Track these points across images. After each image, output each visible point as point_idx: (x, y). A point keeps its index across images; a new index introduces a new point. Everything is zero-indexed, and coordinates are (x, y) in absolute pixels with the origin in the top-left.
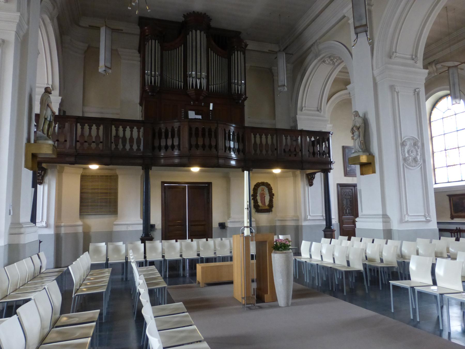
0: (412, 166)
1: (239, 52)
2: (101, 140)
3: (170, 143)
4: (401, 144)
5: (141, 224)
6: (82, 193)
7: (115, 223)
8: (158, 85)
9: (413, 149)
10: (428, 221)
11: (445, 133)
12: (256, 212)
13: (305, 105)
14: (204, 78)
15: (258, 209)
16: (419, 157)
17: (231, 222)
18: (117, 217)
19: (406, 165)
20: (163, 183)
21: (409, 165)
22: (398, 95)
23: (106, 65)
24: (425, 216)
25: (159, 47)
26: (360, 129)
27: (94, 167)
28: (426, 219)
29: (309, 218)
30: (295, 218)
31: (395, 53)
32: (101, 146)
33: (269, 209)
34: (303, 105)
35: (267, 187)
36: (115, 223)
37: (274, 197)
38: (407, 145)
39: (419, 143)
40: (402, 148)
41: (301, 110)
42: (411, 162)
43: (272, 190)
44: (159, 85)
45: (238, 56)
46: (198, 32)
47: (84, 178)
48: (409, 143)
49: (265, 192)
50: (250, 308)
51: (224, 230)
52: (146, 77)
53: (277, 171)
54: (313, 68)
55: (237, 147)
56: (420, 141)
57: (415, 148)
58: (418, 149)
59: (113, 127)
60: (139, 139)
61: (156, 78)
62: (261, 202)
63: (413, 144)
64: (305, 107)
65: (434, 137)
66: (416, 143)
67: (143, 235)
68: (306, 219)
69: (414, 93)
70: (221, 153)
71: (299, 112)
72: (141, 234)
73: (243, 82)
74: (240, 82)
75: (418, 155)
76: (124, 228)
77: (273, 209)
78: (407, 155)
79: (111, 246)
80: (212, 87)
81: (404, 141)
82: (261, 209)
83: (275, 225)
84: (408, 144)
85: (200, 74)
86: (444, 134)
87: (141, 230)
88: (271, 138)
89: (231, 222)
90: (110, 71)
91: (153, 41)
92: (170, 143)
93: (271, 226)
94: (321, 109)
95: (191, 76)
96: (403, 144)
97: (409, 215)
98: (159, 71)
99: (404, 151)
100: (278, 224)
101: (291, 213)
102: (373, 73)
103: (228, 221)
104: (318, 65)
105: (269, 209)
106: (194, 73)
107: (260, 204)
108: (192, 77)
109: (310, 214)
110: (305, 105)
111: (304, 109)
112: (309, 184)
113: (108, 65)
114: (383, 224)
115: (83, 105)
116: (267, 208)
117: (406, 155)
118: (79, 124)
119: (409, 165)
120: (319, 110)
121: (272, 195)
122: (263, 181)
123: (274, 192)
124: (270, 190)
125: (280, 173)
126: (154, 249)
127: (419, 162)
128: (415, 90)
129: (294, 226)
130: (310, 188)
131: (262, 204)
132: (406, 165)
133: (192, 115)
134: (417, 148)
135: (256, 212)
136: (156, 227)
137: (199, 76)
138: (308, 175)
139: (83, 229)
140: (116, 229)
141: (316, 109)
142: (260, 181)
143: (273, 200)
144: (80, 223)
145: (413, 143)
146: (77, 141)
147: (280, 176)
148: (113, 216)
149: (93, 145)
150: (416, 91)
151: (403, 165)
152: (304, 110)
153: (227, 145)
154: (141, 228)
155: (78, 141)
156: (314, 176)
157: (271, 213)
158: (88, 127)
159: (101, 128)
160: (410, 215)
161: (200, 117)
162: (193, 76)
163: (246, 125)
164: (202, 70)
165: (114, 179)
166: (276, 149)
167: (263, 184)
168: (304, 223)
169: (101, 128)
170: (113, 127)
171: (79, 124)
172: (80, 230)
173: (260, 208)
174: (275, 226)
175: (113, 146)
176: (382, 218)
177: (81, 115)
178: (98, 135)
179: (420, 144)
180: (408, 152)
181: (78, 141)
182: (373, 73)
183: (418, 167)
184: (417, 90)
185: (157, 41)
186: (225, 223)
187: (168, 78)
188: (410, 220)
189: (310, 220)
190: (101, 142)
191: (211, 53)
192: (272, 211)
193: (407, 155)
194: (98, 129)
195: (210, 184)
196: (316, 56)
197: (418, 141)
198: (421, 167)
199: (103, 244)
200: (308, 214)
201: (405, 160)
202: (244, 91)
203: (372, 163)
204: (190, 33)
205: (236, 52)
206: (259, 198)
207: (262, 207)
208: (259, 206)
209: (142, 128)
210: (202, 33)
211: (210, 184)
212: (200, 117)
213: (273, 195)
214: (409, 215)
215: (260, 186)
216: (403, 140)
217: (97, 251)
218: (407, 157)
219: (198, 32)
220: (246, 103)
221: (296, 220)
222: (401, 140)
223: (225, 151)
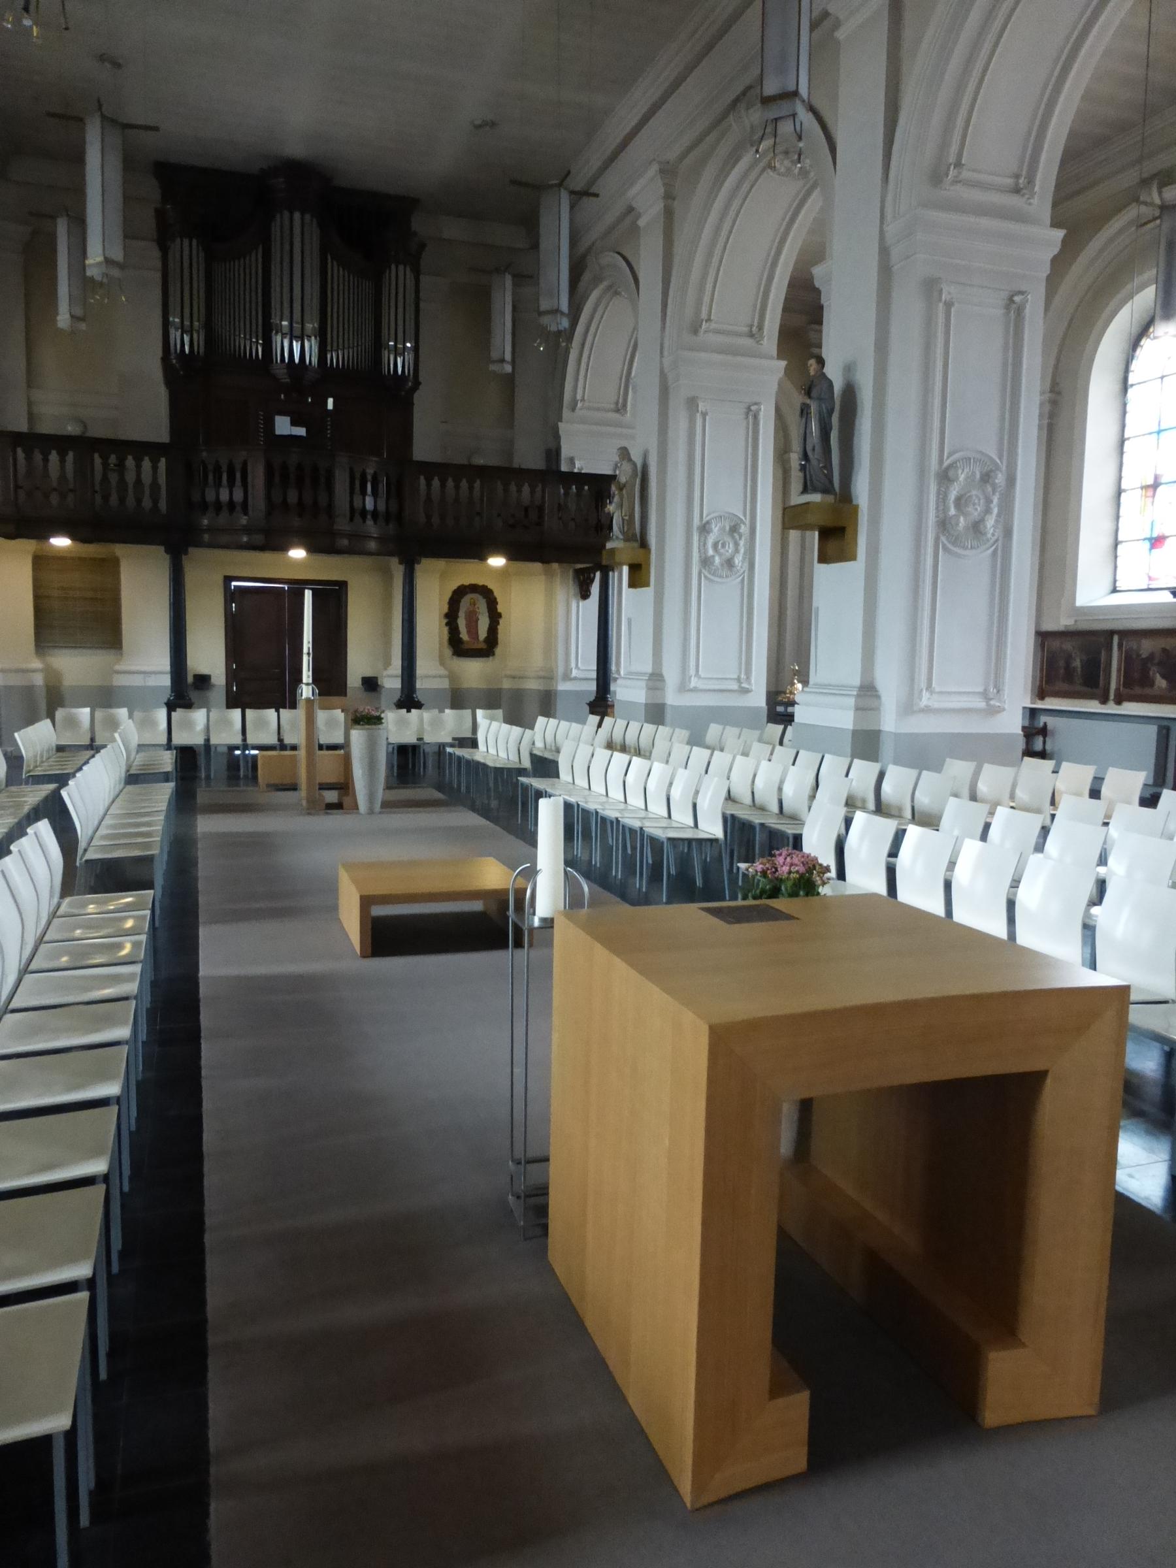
0: (721, 577)
1: (401, 267)
2: (71, 486)
3: (224, 496)
4: (698, 528)
5: (167, 673)
6: (37, 598)
7: (117, 667)
8: (198, 352)
9: (728, 539)
10: (746, 691)
11: (1162, 428)
12: (453, 655)
13: (583, 396)
14: (309, 334)
15: (458, 647)
16: (738, 560)
17: (389, 676)
18: (122, 654)
19: (946, 542)
20: (228, 579)
21: (956, 541)
22: (704, 420)
23: (73, 313)
24: (739, 680)
25: (202, 254)
26: (624, 492)
27: (61, 542)
28: (988, 704)
29: (575, 673)
30: (542, 674)
31: (706, 321)
32: (70, 498)
33: (489, 648)
34: (579, 397)
35: (484, 598)
36: (117, 667)
37: (501, 621)
38: (957, 479)
39: (1000, 475)
40: (942, 489)
41: (573, 409)
42: (719, 567)
43: (497, 603)
44: (202, 350)
45: (398, 276)
46: (297, 216)
47: (41, 562)
48: (968, 473)
49: (478, 608)
50: (309, 814)
51: (373, 694)
52: (172, 331)
53: (497, 562)
54: (595, 310)
55: (382, 507)
56: (748, 522)
57: (733, 537)
58: (740, 539)
59: (96, 456)
60: (155, 485)
61: (195, 336)
62: (469, 632)
63: (978, 476)
64: (583, 400)
65: (1128, 439)
66: (992, 474)
67: (171, 696)
68: (567, 677)
69: (747, 414)
70: (342, 524)
71: (566, 413)
72: (167, 695)
73: (408, 345)
74: (400, 346)
75: (738, 552)
76: (136, 681)
77: (498, 651)
78: (711, 552)
79: (99, 714)
80: (333, 358)
81: (708, 523)
82: (467, 649)
83: (499, 687)
84: (962, 477)
85: (300, 326)
86: (1159, 432)
87: (165, 687)
88: (469, 488)
89: (389, 676)
90: (83, 326)
91: (186, 242)
92: (224, 496)
93: (490, 689)
94: (1031, 181)
95: (279, 329)
96: (704, 529)
97: (699, 677)
98: (203, 318)
99: (705, 544)
100: (506, 685)
101: (537, 661)
102: (661, 363)
103: (385, 673)
104: (604, 302)
105: (489, 648)
106: (285, 323)
107: (464, 635)
108: (283, 334)
109: (579, 665)
110: (583, 396)
111: (579, 405)
112: (581, 593)
113: (78, 312)
114: (646, 692)
115: (29, 385)
116: (483, 646)
117: (949, 510)
118: (19, 451)
119: (713, 575)
120: (620, 408)
121: (495, 617)
122: (473, 582)
123: (500, 608)
124: (492, 603)
125: (492, 556)
126: (189, 725)
127: (738, 568)
128: (749, 409)
129: (539, 690)
130: (581, 603)
131: (469, 637)
132: (946, 542)
133: (283, 426)
134: (989, 489)
135: (453, 655)
136: (213, 680)
137: (297, 332)
138: (578, 573)
139: (46, 679)
140: (120, 681)
141: (613, 406)
142: (467, 582)
143: (497, 629)
144: (37, 664)
145: (981, 472)
146: (17, 487)
147: (502, 573)
148: (113, 651)
149: (54, 499)
150: (751, 410)
151: (700, 573)
152: (581, 409)
153: (357, 503)
154: (166, 681)
155: (21, 488)
156: (592, 575)
157: (491, 658)
158: (41, 456)
159: (70, 456)
160: (937, 689)
161: (301, 431)
162: (284, 332)
163: (424, 448)
164: (307, 317)
165: (111, 566)
166: (478, 514)
167: (474, 588)
168: (562, 686)
169: (70, 456)
170: (96, 456)
171: (19, 451)
172: (39, 680)
173: (466, 646)
174: (500, 691)
175: (98, 499)
176: (649, 680)
177: (23, 427)
178: (63, 477)
179: (1000, 479)
180: (715, 546)
181: (21, 488)
182: (882, 233)
183: (988, 549)
184: (752, 408)
185: (194, 242)
186: (376, 678)
187: (230, 328)
188: (936, 705)
189: (575, 679)
190: (71, 490)
191: (333, 268)
192: (493, 654)
193: (711, 552)
194: (62, 461)
195: (343, 585)
196: (597, 280)
197: (998, 468)
198: (743, 580)
199: (88, 710)
200: (573, 665)
201: (706, 562)
202: (411, 369)
203: (643, 566)
204: (278, 216)
205: (393, 267)
206: (462, 623)
207: (468, 642)
208: (460, 641)
209: (163, 460)
210: (307, 217)
211: (343, 585)
212: (301, 431)
213: (500, 615)
214: (699, 677)
215: (466, 594)
216: (946, 464)
217: (72, 723)
218: (951, 518)
219: (297, 216)
220: (417, 397)
221: (544, 678)
222: (941, 461)
223: (351, 519)
